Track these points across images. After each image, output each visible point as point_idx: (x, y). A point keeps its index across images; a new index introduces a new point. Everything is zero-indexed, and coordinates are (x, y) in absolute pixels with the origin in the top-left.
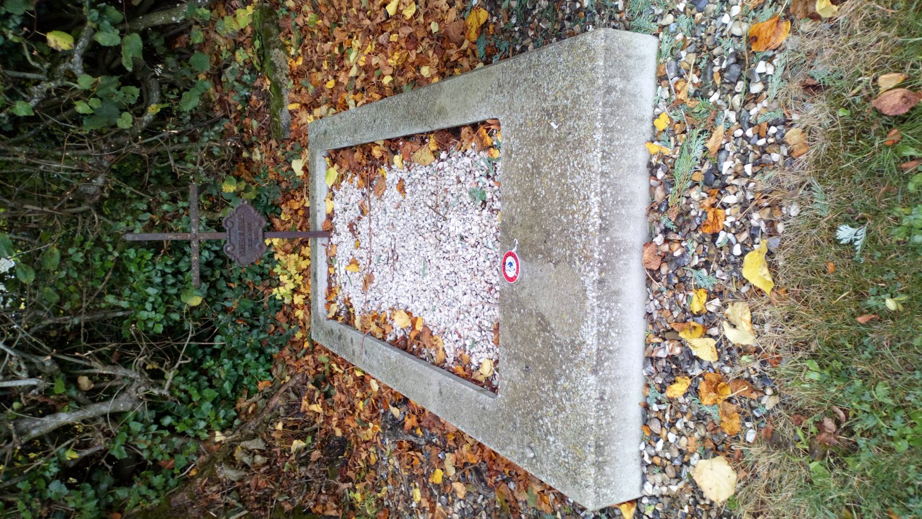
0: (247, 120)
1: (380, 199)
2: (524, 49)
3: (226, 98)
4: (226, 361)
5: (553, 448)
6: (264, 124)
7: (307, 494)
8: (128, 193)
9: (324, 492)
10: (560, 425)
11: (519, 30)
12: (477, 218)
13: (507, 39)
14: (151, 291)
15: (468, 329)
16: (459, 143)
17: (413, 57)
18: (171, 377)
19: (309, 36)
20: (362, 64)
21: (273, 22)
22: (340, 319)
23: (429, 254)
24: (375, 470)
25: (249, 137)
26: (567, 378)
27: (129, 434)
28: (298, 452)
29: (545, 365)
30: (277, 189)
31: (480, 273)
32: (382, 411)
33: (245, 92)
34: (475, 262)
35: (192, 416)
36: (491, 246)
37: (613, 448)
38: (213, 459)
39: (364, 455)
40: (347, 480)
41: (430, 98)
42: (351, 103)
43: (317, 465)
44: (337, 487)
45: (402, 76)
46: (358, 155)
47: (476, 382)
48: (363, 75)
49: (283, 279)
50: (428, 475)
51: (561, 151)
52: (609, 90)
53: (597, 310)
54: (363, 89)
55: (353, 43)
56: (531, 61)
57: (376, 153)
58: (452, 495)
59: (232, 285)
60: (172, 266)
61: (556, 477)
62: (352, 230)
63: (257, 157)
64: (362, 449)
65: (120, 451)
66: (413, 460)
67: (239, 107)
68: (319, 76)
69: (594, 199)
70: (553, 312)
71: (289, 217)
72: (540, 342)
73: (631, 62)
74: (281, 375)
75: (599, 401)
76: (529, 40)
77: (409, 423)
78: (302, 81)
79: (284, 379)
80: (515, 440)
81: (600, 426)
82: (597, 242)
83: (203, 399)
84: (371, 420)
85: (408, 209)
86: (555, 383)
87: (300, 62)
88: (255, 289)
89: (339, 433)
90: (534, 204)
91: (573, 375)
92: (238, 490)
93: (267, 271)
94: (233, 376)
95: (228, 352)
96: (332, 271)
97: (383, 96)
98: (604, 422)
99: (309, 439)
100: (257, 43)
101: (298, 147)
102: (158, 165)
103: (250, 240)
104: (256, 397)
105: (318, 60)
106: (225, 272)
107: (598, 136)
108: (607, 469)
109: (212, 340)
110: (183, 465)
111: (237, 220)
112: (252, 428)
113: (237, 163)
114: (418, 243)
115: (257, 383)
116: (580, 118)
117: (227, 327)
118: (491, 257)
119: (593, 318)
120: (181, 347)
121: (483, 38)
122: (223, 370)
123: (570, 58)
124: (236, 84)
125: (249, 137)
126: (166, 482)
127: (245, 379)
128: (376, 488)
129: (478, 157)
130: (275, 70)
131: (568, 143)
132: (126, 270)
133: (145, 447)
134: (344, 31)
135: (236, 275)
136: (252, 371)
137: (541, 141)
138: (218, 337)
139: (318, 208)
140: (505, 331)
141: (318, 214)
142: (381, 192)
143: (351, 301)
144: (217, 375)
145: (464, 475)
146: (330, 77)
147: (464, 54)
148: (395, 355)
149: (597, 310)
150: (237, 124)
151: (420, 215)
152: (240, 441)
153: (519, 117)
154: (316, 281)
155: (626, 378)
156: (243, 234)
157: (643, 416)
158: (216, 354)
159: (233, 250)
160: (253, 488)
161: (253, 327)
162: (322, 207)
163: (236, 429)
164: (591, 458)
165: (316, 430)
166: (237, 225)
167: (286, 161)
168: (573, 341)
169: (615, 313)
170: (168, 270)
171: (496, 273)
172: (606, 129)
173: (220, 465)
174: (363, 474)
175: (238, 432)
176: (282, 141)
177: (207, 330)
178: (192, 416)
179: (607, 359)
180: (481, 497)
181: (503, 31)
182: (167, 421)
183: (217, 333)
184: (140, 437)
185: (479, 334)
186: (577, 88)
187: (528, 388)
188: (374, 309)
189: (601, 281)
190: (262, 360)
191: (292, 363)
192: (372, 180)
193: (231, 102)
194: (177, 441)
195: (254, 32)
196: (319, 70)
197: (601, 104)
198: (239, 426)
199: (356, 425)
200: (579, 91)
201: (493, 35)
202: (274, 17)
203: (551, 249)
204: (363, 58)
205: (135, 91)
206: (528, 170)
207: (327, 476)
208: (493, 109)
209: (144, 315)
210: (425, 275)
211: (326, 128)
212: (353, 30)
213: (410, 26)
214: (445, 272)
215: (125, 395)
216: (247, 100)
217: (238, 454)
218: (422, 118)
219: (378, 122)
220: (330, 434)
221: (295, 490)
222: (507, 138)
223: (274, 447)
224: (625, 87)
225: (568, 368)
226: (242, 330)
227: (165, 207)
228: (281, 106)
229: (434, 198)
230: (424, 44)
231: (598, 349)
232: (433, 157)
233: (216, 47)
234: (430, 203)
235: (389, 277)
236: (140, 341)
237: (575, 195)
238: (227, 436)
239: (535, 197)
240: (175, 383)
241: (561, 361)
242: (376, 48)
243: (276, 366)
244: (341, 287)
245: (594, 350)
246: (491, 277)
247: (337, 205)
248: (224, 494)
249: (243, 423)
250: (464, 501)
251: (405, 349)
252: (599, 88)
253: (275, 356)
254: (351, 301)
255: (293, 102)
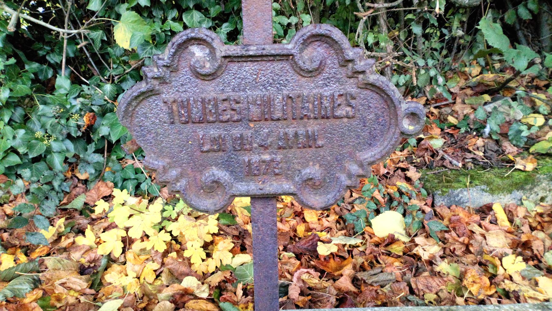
6: (443, 159)
103: (241, 145)
111: (333, 89)
166: (308, 88)
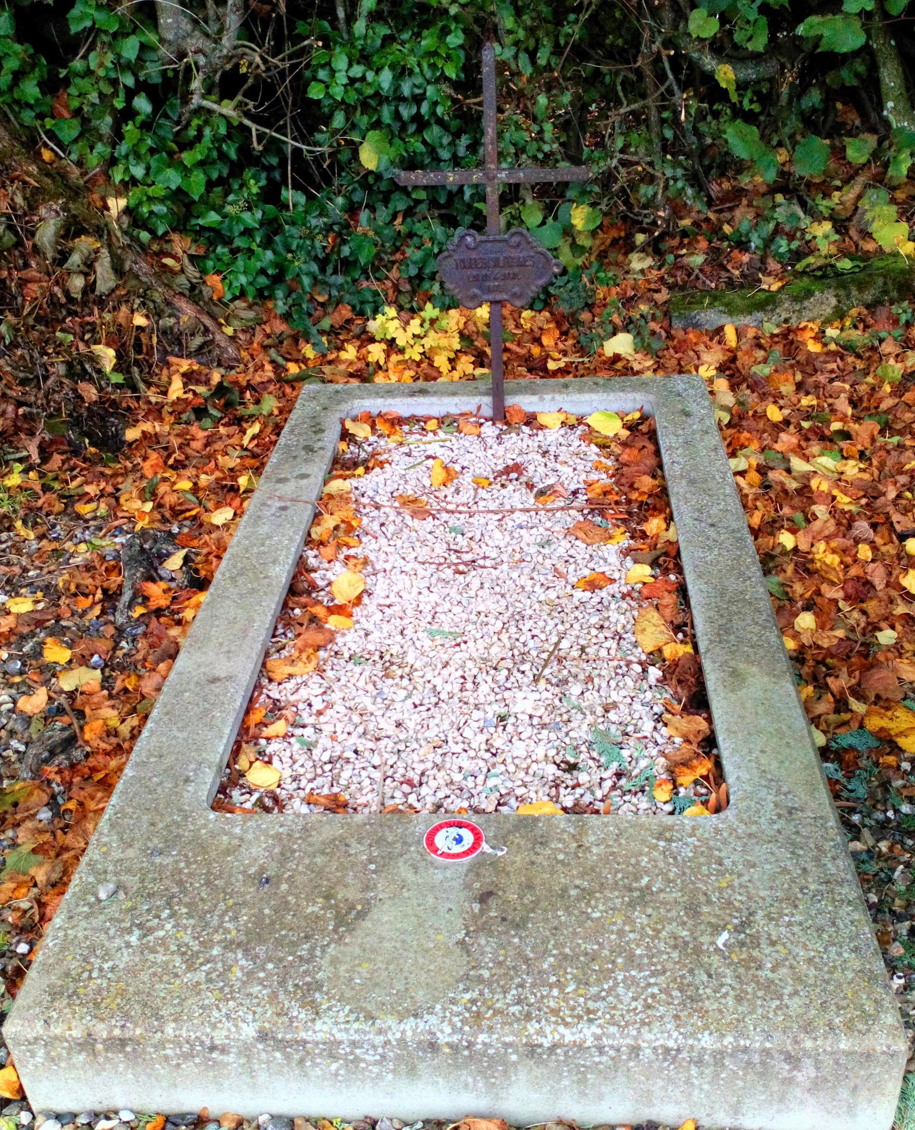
0: (703, 244)
1: (568, 532)
2: (854, 831)
3: (745, 202)
4: (259, 215)
5: (118, 942)
6: (697, 278)
7: (16, 378)
8: (567, 29)
9: (21, 411)
10: (160, 958)
11: (888, 820)
12: (540, 752)
13: (872, 795)
14: (386, 78)
15: (334, 732)
16: (679, 708)
17: (831, 593)
18: (225, 111)
19: (860, 365)
20: (814, 484)
21: (885, 292)
22: (343, 446)
23: (470, 643)
24: (63, 512)
25: (671, 250)
26: (250, 974)
27: (115, 35)
28: (93, 359)
29: (273, 923)
30: (579, 304)
31: (438, 760)
32: (175, 530)
33: (755, 242)
34: (458, 748)
35: (152, 151)
36: (491, 783)
37: (121, 1067)
38: (75, 193)
39: (92, 490)
40: (45, 453)
41: (761, 652)
42: (739, 463)
43: (71, 395)
44: (31, 433)
45: (796, 571)
46: (647, 483)
47: (236, 752)
48: (793, 485)
49: (415, 326)
50: (57, 632)
51: (675, 955)
52: (793, 1060)
53: (379, 1040)
54: (767, 487)
55: (852, 462)
56: (840, 884)
57: (654, 525)
58: (23, 682)
59: (399, 220)
60: (433, 113)
61: (63, 949)
62: (507, 470)
63: (638, 262)
64: (103, 484)
65: (81, 19)
66: (86, 596)
67: (727, 229)
68: (787, 388)
69: (588, 1033)
70: (372, 940)
71: (527, 326)
72: (316, 909)
73: (844, 1094)
74: (236, 317)
75: (208, 1043)
76: (871, 842)
77: (155, 590)
78: (778, 350)
79: (228, 324)
80: (131, 853)
81: (161, 1045)
82: (509, 1039)
83: (186, 171)
84: (159, 506)
85: (552, 595)
86: (239, 945)
87: (814, 347)
88: (393, 262)
89: (131, 434)
90: (573, 892)
91: (256, 989)
92: (19, 244)
93: (426, 285)
94: (230, 229)
95: (276, 219)
96: (431, 425)
97: (756, 533)
98: (169, 1052)
99: (118, 378)
100: (845, 264)
101: (656, 345)
102: (619, 80)
103: (486, 278)
104: (192, 271)
105: (817, 386)
106: (423, 207)
107: (707, 1041)
108: (82, 1057)
109: (296, 186)
110: (60, 135)
112: (135, 267)
113: (624, 226)
114: (491, 619)
115: (218, 272)
116: (739, 999)
117: (321, 215)
118: (470, 783)
119: (365, 1033)
120: (281, 130)
121: (874, 743)
122: (241, 211)
123: (850, 975)
124: (771, 226)
125: (671, 250)
126: (31, 107)
127: (226, 250)
128: (32, 516)
129: (654, 752)
130: (796, 299)
131: (691, 971)
132: (426, 25)
133: (93, 66)
134: (873, 440)
135: (419, 228)
136: (240, 262)
137: (693, 910)
138: (302, 199)
139: (548, 397)
140: (332, 827)
141: (535, 398)
142: (581, 535)
143: (377, 470)
144: (231, 198)
145: (60, 711)
146: (786, 412)
147: (841, 705)
148: (281, 574)
149: (379, 1040)
150: (695, 224)
151: (541, 624)
152: (110, 246)
153: (735, 857)
154: (412, 394)
155: (253, 1086)
156: (496, 266)
157: (183, 1116)
158: (270, 195)
159: (468, 247)
160: (24, 274)
161: (323, 264)
162: (548, 404)
163: (132, 238)
164: (101, 1030)
165: (135, 389)
166: (514, 253)
167: (631, 321)
168: (319, 986)
169: (375, 1069)
170: (425, 108)
171: (441, 794)
172: (719, 1056)
173: (65, 208)
174: (57, 485)
175: (126, 240)
176: (666, 312)
177: (312, 177)
178: (152, 151)
179: (288, 1057)
180: (22, 748)
181: (885, 785)
182: (142, 104)
183: (310, 197)
184: (110, 56)
185: (326, 757)
186: (796, 993)
187: (228, 883)
188: (365, 520)
189: (433, 1046)
190: (263, 281)
191: (259, 337)
192: (602, 513)
193: (738, 213)
194: (105, 124)
195: (866, 256)
196: (799, 386)
197: (768, 1045)
198: (136, 239)
199: (149, 473)
200: (791, 996)
201: (877, 764)
202: (895, 294)
203: (490, 933)
204: (825, 487)
205: (759, 44)
206: (637, 879)
207: (51, 416)
208: (748, 797)
209: (341, 62)
210: (432, 635)
211: (695, 404)
212: (875, 462)
213: (888, 585)
214: (438, 681)
215: (189, 27)
216: (742, 245)
217: (85, 244)
218: (723, 631)
219: (711, 532)
220: (129, 417)
221: (22, 357)
222: (694, 828)
223: (102, 310)
224: (798, 1084)
225: (269, 975)
226: (318, 244)
227: (542, 100)
228: (731, 310)
229: (575, 653)
230: (856, 615)
231: (305, 1042)
232: (649, 649)
233: (838, 183)
234: (565, 644)
235: (423, 553)
236: (290, 57)
237: (594, 990)
238: (118, 219)
239: (586, 894)
240: (215, 119)
241: (281, 960)
242: (843, 512)
243: (250, 307)
244: (401, 444)
245: (303, 1035)
246: (433, 784)
247: (553, 435)
248: (9, 218)
249: (142, 246)
250: (12, 711)
251: (293, 591)
252: (796, 1042)
253: (270, 305)
254: (377, 470)
255: (739, 334)
